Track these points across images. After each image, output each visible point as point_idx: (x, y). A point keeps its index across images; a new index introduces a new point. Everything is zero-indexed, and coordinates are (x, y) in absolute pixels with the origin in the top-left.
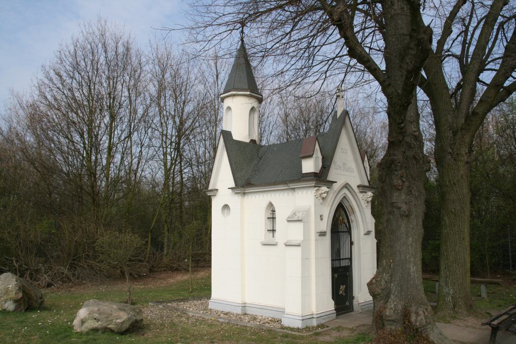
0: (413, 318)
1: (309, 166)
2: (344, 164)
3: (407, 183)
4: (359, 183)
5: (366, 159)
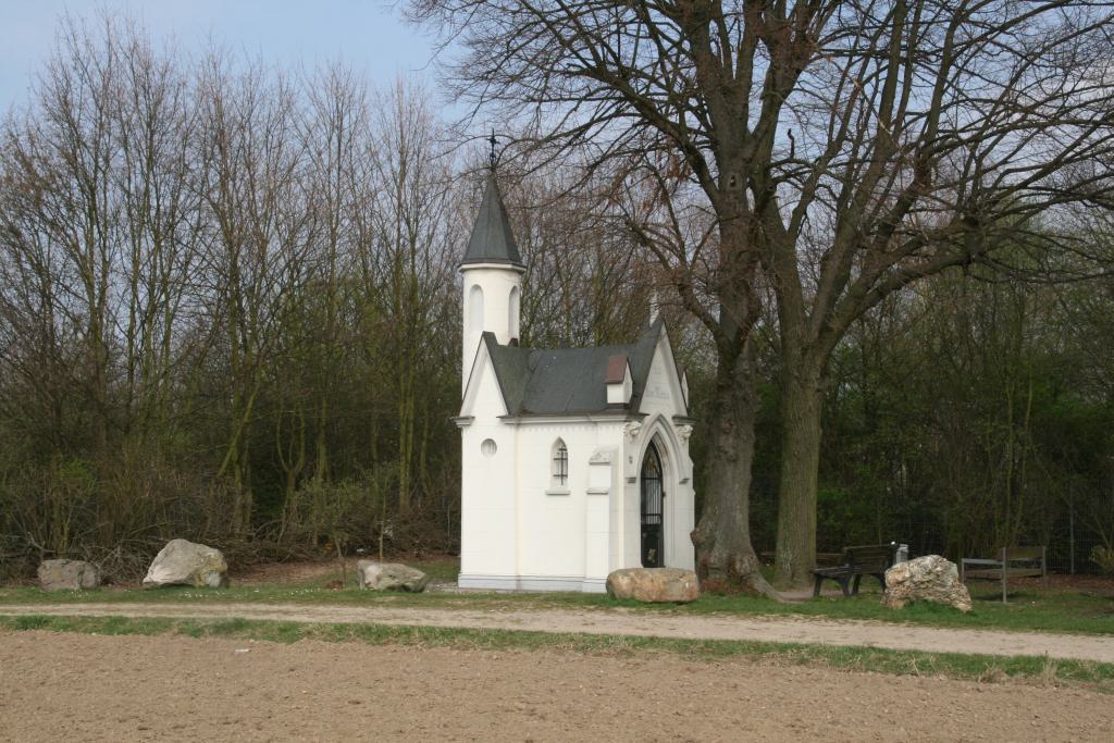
0: (738, 566)
1: (617, 394)
2: (657, 389)
3: (735, 427)
4: (674, 413)
5: (684, 377)
